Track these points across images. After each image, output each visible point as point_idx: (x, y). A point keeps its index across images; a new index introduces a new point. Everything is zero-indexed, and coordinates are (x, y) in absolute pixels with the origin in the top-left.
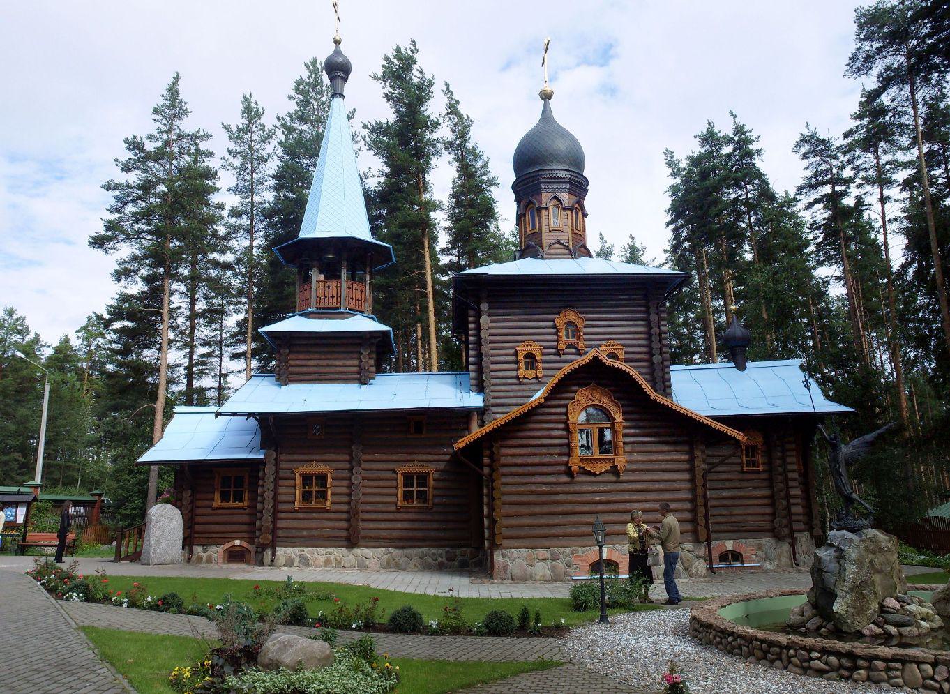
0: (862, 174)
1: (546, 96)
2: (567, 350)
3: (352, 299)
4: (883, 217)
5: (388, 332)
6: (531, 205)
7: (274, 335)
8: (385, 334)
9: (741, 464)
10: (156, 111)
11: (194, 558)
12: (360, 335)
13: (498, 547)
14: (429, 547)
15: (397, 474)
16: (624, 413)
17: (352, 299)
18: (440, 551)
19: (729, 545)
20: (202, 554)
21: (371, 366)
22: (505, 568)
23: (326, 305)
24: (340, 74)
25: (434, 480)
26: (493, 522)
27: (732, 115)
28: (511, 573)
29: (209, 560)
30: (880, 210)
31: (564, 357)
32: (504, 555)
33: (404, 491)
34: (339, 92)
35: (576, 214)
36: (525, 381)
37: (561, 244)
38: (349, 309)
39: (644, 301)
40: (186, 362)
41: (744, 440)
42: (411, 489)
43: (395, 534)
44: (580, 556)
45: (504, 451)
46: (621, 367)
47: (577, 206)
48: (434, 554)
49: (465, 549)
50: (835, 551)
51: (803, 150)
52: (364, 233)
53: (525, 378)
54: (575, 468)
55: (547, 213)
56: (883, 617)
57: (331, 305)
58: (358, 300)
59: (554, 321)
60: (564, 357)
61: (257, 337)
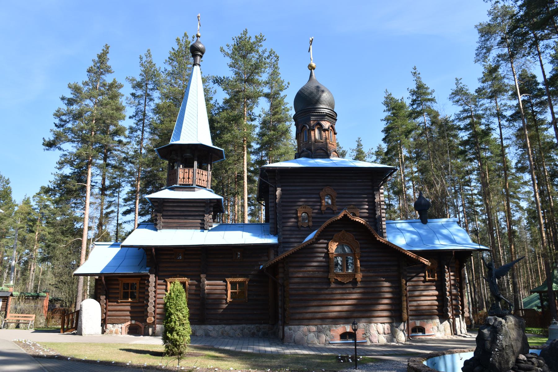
1: (311, 68)
2: (326, 211)
3: (200, 179)
4: (501, 138)
5: (221, 199)
6: (305, 128)
7: (152, 200)
8: (219, 200)
9: (425, 277)
11: (107, 331)
12: (205, 201)
14: (246, 324)
17: (200, 179)
18: (253, 326)
20: (112, 329)
21: (211, 219)
24: (200, 54)
26: (285, 310)
27: (140, 58)
31: (324, 216)
33: (231, 292)
35: (331, 132)
36: (302, 229)
37: (323, 150)
38: (197, 185)
39: (370, 183)
40: (98, 215)
41: (429, 265)
46: (360, 221)
47: (331, 128)
48: (249, 328)
49: (265, 325)
50: (491, 328)
51: (457, 98)
52: (208, 142)
53: (302, 226)
55: (314, 132)
56: (517, 366)
57: (187, 183)
58: (204, 180)
60: (324, 216)
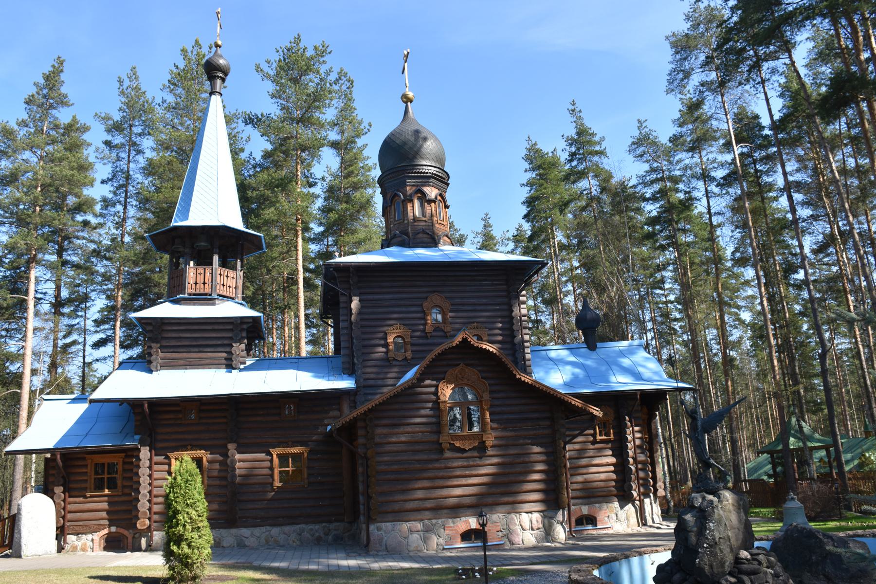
0: (689, 172)
4: (709, 212)
5: (258, 318)
6: (397, 198)
8: (256, 320)
10: (28, 102)
11: (67, 547)
13: (374, 521)
15: (272, 455)
16: (491, 392)
18: (317, 527)
19: (585, 510)
21: (242, 351)
22: (381, 540)
23: (198, 291)
25: (208, 461)
26: (369, 498)
28: (386, 545)
29: (84, 550)
30: (706, 205)
32: (379, 529)
34: (218, 90)
35: (439, 205)
36: (394, 363)
40: (50, 350)
41: (601, 416)
42: (106, 480)
43: (584, 471)
44: (451, 527)
45: (379, 431)
47: (439, 198)
48: (312, 529)
53: (394, 359)
54: (445, 445)
57: (202, 291)
59: (421, 305)
61: (127, 324)
